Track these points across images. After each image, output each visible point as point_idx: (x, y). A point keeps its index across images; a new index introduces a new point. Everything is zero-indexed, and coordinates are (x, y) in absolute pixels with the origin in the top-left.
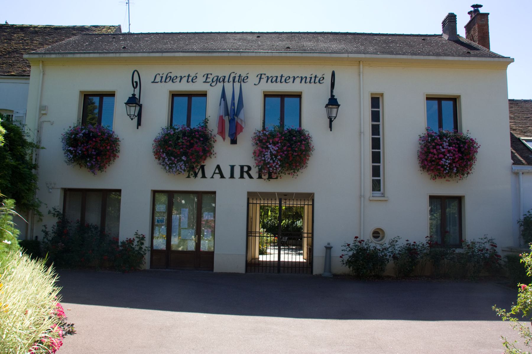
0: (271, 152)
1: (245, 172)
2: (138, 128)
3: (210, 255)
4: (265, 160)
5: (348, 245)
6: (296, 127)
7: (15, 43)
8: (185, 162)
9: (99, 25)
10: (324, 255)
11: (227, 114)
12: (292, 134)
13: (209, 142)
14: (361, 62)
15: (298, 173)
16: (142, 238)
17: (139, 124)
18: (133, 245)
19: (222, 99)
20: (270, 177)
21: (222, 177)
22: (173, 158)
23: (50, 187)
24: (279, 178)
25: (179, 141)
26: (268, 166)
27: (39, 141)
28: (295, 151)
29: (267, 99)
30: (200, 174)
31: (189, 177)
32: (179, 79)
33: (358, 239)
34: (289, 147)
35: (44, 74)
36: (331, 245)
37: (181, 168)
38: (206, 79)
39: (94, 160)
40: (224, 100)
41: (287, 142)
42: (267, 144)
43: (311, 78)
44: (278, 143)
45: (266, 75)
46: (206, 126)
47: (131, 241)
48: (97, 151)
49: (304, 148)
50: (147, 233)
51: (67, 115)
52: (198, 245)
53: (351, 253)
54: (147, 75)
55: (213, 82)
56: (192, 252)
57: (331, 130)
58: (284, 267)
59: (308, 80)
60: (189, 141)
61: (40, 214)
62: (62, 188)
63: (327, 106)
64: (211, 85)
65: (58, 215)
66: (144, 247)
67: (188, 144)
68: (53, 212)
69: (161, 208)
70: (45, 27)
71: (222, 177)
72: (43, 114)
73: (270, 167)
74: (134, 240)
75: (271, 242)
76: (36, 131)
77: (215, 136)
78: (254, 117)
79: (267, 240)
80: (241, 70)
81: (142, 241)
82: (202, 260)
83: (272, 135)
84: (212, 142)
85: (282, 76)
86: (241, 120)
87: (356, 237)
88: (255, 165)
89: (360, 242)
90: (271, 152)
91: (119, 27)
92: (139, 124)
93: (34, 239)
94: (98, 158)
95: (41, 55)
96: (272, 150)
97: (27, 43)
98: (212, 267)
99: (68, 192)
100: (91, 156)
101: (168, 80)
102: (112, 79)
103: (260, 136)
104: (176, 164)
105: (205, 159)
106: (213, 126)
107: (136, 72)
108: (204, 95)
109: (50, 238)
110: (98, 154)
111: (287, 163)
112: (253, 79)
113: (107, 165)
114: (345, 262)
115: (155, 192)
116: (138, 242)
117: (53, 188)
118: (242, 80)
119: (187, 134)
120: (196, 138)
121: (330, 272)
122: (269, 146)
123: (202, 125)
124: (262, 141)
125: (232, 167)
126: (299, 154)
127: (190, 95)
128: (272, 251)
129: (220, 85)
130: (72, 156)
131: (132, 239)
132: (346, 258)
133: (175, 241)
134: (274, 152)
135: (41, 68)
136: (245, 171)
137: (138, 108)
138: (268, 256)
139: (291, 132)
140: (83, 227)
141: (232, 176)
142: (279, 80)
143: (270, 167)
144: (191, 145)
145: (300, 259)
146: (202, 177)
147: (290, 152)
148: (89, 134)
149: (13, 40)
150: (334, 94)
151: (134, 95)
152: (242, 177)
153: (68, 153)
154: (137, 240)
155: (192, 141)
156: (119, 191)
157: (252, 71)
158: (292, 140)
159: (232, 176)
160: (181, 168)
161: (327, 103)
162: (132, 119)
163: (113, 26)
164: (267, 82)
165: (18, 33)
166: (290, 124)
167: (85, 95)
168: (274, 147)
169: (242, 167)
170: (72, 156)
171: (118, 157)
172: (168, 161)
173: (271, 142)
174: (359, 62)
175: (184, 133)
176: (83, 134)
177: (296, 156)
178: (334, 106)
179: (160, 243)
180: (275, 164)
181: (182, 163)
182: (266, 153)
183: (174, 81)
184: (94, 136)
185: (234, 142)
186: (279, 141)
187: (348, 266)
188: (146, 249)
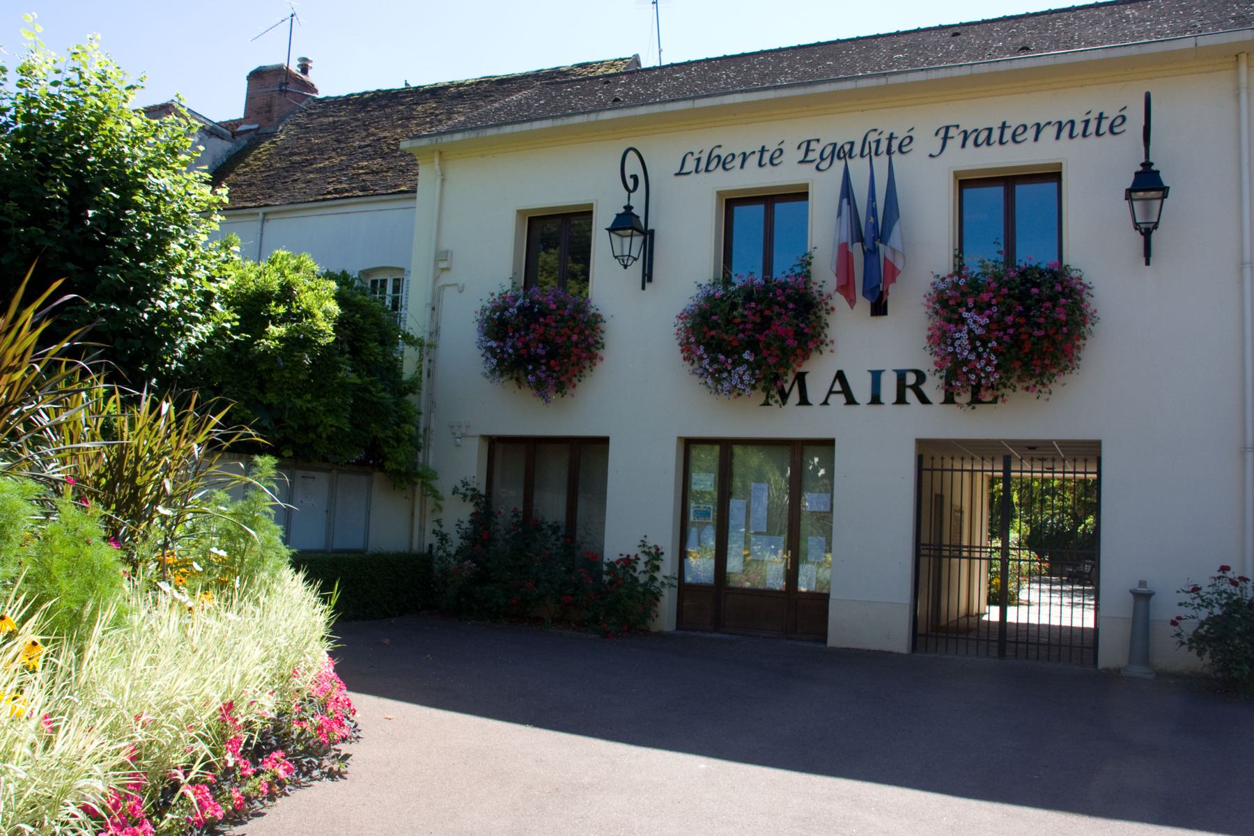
0: (970, 331)
1: (911, 387)
2: (643, 288)
3: (820, 600)
4: (954, 353)
5: (1196, 589)
6: (1044, 259)
7: (417, 125)
8: (752, 366)
9: (590, 60)
10: (1129, 615)
11: (858, 236)
12: (1027, 281)
13: (815, 313)
14: (1243, 57)
15: (1053, 386)
16: (655, 556)
17: (647, 276)
18: (635, 570)
19: (845, 201)
20: (976, 400)
21: (851, 401)
22: (722, 357)
23: (458, 434)
24: (1000, 400)
25: (735, 313)
26: (965, 369)
27: (435, 332)
28: (1039, 326)
29: (968, 192)
30: (794, 396)
31: (766, 404)
32: (738, 161)
33: (1229, 574)
34: (1020, 314)
35: (443, 180)
36: (1151, 587)
37: (742, 381)
38: (806, 155)
39: (544, 368)
40: (849, 203)
41: (1015, 303)
42: (962, 310)
43: (1087, 122)
44: (989, 306)
45: (962, 129)
46: (809, 272)
47: (628, 562)
48: (548, 348)
49: (1063, 317)
50: (665, 539)
51: (490, 265)
52: (792, 575)
53: (1204, 614)
54: (663, 154)
55: (822, 159)
56: (780, 592)
57: (1148, 263)
58: (1049, 645)
59: (1079, 128)
60: (762, 312)
61: (436, 495)
62: (483, 437)
63: (1129, 194)
64: (818, 168)
65: (475, 497)
66: (659, 576)
67: (758, 320)
68: (463, 490)
69: (704, 482)
70: (479, 83)
71: (851, 401)
72: (443, 269)
73: (970, 372)
74: (637, 558)
75: (1030, 573)
76: (429, 309)
77: (830, 296)
78: (931, 241)
79: (1019, 567)
80: (892, 122)
81: (656, 563)
82: (801, 613)
83: (975, 286)
84: (823, 313)
85: (1003, 127)
86: (894, 251)
87: (1224, 569)
88: (934, 368)
89: (1234, 583)
90: (970, 331)
91: (636, 60)
92: (647, 276)
93: (426, 550)
94: (552, 362)
95: (434, 139)
96: (973, 326)
97: (440, 121)
98: (823, 636)
99: (495, 444)
100: (535, 360)
101: (712, 167)
102: (577, 175)
103: (942, 291)
104: (729, 372)
105: (806, 357)
106: (825, 274)
107: (631, 154)
108: (800, 195)
109: (453, 551)
110: (551, 355)
111: (1018, 359)
112: (926, 142)
113: (575, 380)
114: (1185, 640)
115: (689, 444)
116: (646, 563)
117: (463, 436)
118: (899, 146)
119: (755, 295)
120: (778, 303)
121: (1146, 659)
122: (965, 315)
123: (798, 270)
124: (950, 303)
125: (876, 376)
126: (1051, 333)
127: (768, 199)
128: (1034, 597)
129: (839, 165)
130: (495, 361)
131: (632, 557)
132: (1188, 628)
133: (734, 564)
134: (978, 331)
135: (437, 167)
136: (909, 387)
137: (638, 240)
138: (1023, 609)
139: (1029, 277)
140: (528, 523)
141: (876, 400)
142: (995, 136)
143: (970, 372)
144: (765, 323)
145: (1083, 618)
146: (801, 403)
147: (1023, 330)
148: (531, 307)
149: (414, 118)
150: (1151, 160)
151: (628, 208)
152: (901, 400)
153: (489, 355)
154: (644, 558)
155: (767, 313)
156: (605, 441)
157: (920, 121)
158: (1030, 297)
159: (876, 400)
160: (742, 381)
161: (1129, 186)
162: (626, 267)
163: (621, 59)
164: (963, 146)
165: (425, 101)
166: (1031, 253)
167: (530, 219)
168: (978, 319)
169: (901, 376)
170: (495, 361)
171: (602, 359)
172: (710, 364)
173: (971, 305)
174: (1235, 56)
175: (748, 294)
176: (519, 308)
177: (1039, 338)
178: (1152, 194)
179: (701, 565)
180: (983, 362)
181: (745, 367)
182: (957, 335)
183: (728, 166)
184: (542, 313)
185: (879, 309)
186: (994, 302)
187: (1194, 651)
188: (666, 581)
